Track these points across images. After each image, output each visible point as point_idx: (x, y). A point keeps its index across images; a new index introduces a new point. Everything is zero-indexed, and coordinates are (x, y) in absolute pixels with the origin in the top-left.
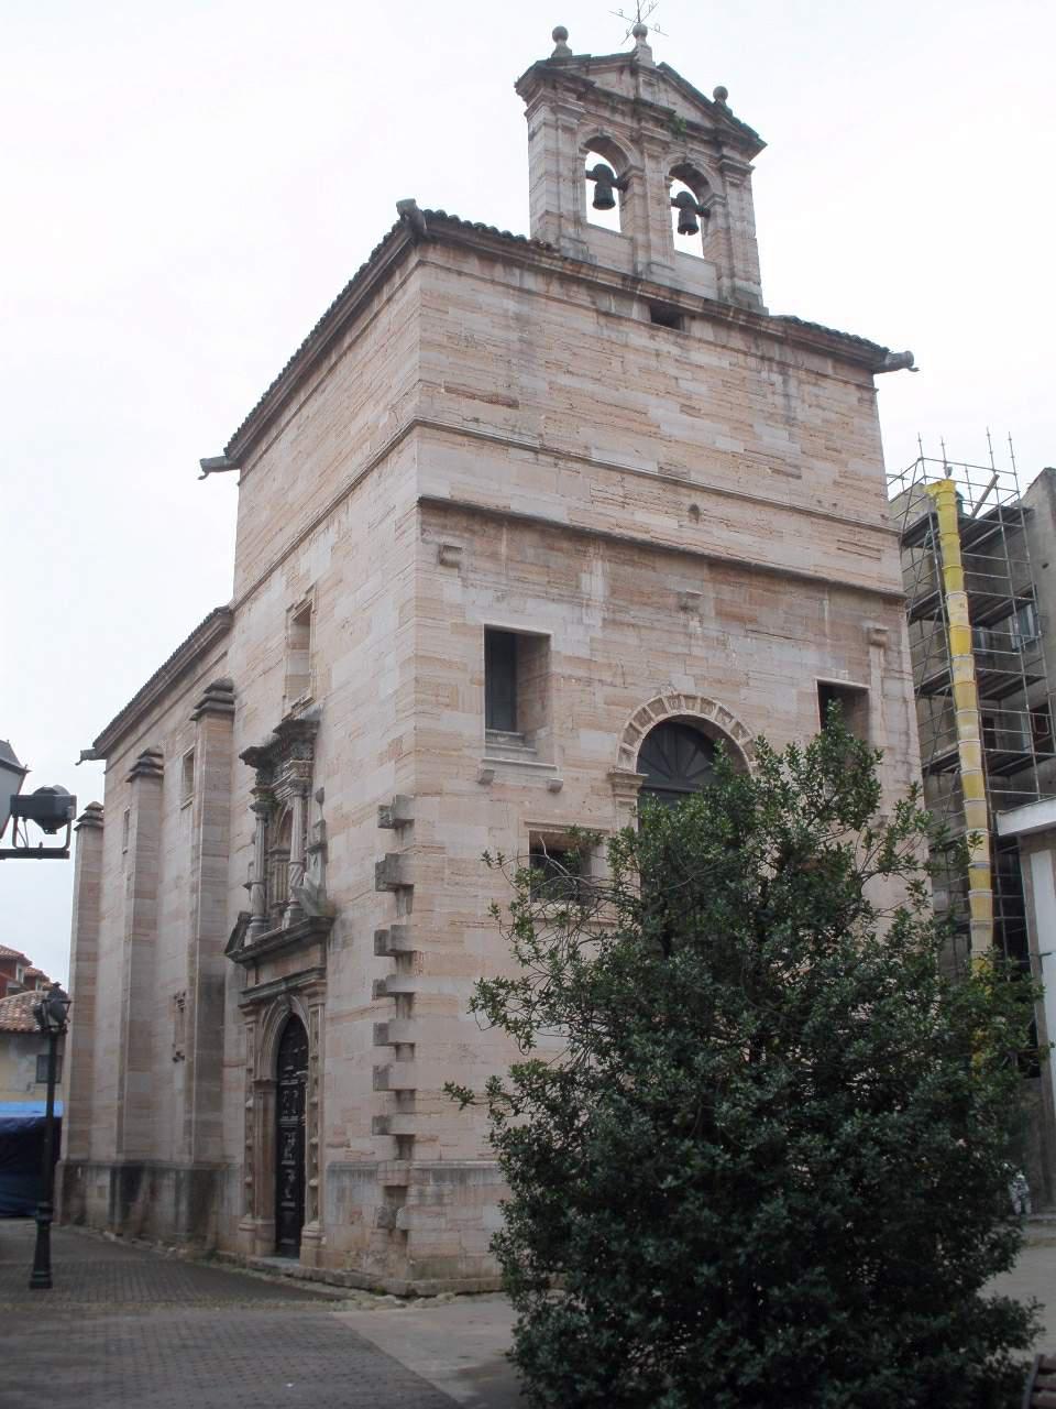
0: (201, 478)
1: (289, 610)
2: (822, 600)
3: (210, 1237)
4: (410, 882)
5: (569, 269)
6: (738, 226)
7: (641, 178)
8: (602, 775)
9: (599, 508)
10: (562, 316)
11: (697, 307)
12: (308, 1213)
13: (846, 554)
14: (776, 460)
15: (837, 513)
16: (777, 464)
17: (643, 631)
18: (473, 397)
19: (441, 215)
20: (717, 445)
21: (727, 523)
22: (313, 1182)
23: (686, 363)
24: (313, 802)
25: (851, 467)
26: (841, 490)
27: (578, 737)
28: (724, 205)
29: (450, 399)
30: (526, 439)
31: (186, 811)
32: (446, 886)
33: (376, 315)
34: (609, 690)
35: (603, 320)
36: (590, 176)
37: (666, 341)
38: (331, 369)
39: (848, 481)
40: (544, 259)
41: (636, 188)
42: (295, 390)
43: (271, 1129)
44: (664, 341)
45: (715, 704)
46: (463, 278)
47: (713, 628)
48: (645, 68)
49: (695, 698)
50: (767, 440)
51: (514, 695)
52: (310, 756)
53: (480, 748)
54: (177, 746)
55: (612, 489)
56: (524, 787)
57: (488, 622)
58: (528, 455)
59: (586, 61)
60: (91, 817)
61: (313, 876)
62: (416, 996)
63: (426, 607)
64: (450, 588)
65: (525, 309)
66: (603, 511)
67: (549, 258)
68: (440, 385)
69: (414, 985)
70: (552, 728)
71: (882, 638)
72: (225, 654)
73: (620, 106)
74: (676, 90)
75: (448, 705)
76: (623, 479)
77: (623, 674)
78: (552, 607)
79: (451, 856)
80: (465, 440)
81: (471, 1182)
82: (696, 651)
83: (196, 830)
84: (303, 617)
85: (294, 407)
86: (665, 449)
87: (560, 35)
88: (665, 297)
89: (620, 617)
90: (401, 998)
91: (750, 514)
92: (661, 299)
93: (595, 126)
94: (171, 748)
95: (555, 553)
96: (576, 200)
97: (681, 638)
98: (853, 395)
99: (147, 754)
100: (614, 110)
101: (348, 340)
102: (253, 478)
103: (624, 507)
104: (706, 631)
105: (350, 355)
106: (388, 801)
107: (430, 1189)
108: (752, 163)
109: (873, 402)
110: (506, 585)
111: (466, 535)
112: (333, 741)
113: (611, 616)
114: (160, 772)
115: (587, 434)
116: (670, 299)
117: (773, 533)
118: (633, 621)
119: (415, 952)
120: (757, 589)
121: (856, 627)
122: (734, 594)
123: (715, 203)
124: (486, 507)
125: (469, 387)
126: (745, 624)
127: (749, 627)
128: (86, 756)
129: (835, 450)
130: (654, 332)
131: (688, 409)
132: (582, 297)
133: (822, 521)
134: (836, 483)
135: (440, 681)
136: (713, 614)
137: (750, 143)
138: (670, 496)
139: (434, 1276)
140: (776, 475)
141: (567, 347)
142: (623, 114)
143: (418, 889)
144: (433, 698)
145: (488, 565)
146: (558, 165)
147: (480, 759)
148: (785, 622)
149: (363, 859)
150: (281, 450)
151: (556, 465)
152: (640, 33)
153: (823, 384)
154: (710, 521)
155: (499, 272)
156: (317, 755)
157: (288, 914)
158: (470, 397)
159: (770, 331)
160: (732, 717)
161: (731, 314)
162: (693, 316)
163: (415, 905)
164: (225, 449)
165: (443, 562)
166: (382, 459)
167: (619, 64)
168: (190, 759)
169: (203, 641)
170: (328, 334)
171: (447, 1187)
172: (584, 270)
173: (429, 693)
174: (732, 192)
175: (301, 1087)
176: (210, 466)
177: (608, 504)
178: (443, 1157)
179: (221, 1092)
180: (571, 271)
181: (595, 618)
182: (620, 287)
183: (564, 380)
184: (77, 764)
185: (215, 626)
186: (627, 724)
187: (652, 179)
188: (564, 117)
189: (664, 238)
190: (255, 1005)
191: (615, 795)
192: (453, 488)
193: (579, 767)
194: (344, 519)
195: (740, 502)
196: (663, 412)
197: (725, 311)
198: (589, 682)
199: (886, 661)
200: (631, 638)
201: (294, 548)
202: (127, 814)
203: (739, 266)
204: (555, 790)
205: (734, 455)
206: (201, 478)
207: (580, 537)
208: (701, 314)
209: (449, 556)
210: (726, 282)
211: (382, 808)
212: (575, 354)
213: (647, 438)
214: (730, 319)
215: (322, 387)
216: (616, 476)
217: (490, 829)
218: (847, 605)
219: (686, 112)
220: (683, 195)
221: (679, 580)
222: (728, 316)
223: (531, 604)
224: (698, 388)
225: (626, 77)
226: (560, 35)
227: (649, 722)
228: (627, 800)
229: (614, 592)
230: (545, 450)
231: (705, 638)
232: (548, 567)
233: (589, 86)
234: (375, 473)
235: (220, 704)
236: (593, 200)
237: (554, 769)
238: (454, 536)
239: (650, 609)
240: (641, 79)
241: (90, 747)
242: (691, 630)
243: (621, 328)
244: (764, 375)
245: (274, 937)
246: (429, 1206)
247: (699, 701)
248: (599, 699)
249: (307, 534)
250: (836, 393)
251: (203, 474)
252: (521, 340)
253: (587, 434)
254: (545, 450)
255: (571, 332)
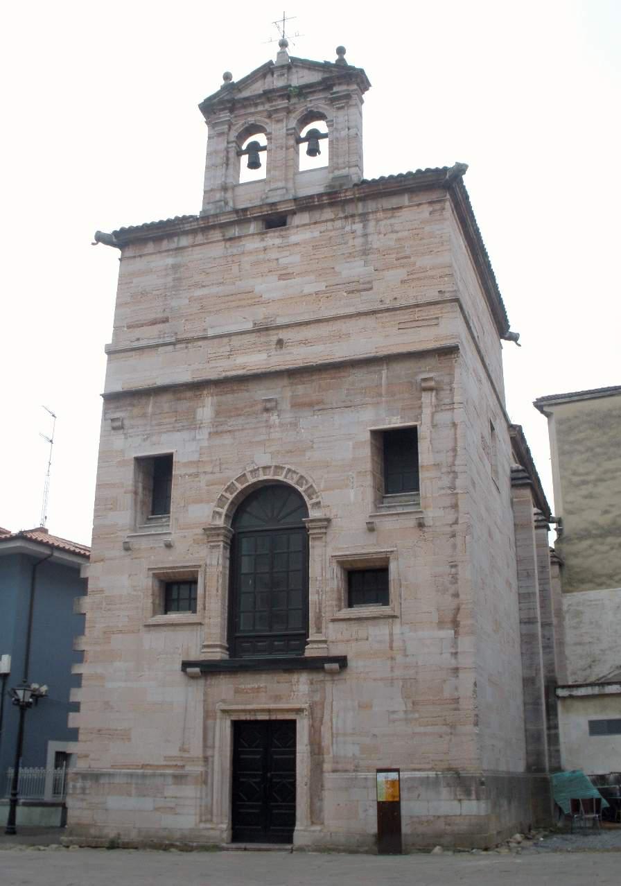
2: (380, 371)
4: (85, 612)
5: (202, 224)
8: (200, 531)
9: (213, 364)
11: (291, 207)
14: (339, 286)
15: (397, 304)
16: (353, 287)
18: (142, 326)
19: (123, 230)
21: (305, 342)
27: (187, 510)
29: (130, 332)
32: (104, 612)
34: (209, 477)
39: (415, 276)
40: (186, 225)
45: (285, 468)
46: (143, 258)
47: (288, 417)
49: (270, 467)
56: (151, 548)
57: (136, 455)
58: (170, 348)
64: (119, 441)
65: (179, 259)
67: (188, 223)
68: (124, 327)
71: (432, 384)
73: (258, 101)
74: (303, 67)
77: (220, 464)
78: (178, 435)
79: (107, 594)
80: (133, 353)
81: (102, 781)
91: (324, 330)
92: (266, 213)
93: (243, 122)
97: (264, 430)
100: (256, 105)
107: (79, 785)
111: (129, 408)
116: (272, 210)
117: (340, 337)
118: (230, 429)
119: (84, 651)
120: (325, 380)
121: (411, 382)
122: (304, 389)
125: (140, 320)
126: (313, 407)
127: (317, 408)
129: (406, 257)
131: (284, 276)
133: (387, 314)
136: (288, 407)
138: (263, 339)
139: (77, 835)
142: (263, 103)
148: (347, 396)
151: (187, 347)
154: (291, 346)
155: (165, 245)
158: (140, 327)
159: (348, 197)
162: (293, 213)
167: (261, 74)
171: (88, 784)
172: (210, 220)
177: (219, 359)
178: (92, 766)
180: (204, 223)
181: (203, 435)
182: (237, 219)
191: (209, 542)
193: (187, 529)
195: (317, 325)
197: (310, 200)
198: (197, 475)
199: (437, 399)
200: (227, 439)
208: (296, 209)
212: (208, 273)
216: (226, 340)
217: (130, 576)
218: (401, 369)
221: (261, 392)
222: (314, 202)
223: (164, 437)
226: (341, 51)
227: (235, 491)
228: (216, 544)
230: (179, 341)
231: (281, 425)
232: (176, 412)
237: (170, 533)
238: (122, 411)
239: (243, 417)
242: (271, 422)
243: (241, 243)
244: (348, 228)
248: (203, 484)
252: (174, 280)
254: (179, 341)
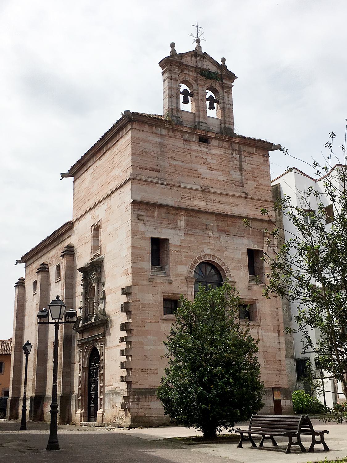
0: (61, 179)
1: (92, 226)
3: (67, 417)
6: (227, 106)
7: (197, 93)
8: (183, 278)
10: (172, 142)
12: (99, 407)
13: (257, 210)
15: (255, 197)
17: (196, 236)
20: (218, 179)
21: (221, 203)
22: (101, 397)
23: (210, 154)
24: (101, 284)
25: (260, 182)
26: (256, 190)
28: (223, 99)
30: (162, 182)
31: (57, 284)
33: (118, 141)
34: (185, 254)
35: (185, 143)
36: (181, 93)
37: (204, 147)
38: (104, 153)
41: (195, 97)
42: (92, 157)
43: (87, 383)
44: (203, 148)
47: (216, 234)
48: (199, 55)
49: (211, 255)
50: (234, 176)
51: (159, 255)
52: (100, 271)
53: (150, 272)
54: (54, 262)
55: (187, 195)
59: (182, 55)
60: (21, 283)
61: (101, 306)
62: (132, 342)
63: (135, 233)
64: (141, 227)
65: (162, 141)
66: (184, 201)
69: (132, 339)
70: (169, 266)
72: (71, 236)
75: (141, 260)
76: (190, 191)
79: (142, 302)
82: (211, 241)
83: (63, 291)
84: (97, 229)
85: (92, 162)
86: (203, 181)
87: (173, 45)
88: (203, 134)
89: (189, 232)
90: (128, 343)
91: (228, 200)
94: (51, 262)
95: (170, 215)
96: (177, 103)
97: (207, 238)
98: (262, 159)
99: (43, 264)
101: (109, 146)
102: (78, 181)
103: (190, 200)
104: (214, 235)
105: (110, 151)
106: (124, 287)
108: (232, 84)
109: (268, 161)
110: (157, 225)
112: (107, 267)
113: (187, 232)
114: (47, 270)
115: (180, 178)
118: (193, 234)
122: (223, 224)
123: (220, 99)
124: (162, 448)
127: (227, 233)
128: (18, 262)
129: (255, 177)
130: (200, 145)
131: (210, 169)
132: (179, 135)
134: (255, 188)
135: (138, 253)
137: (232, 77)
140: (236, 187)
141: (174, 152)
143: (133, 312)
144: (137, 258)
145: (152, 220)
146: (172, 92)
147: (149, 275)
149: (117, 302)
150: (88, 176)
151: (171, 189)
152: (198, 41)
153: (252, 157)
156: (102, 271)
157: (94, 318)
160: (221, 260)
161: (224, 137)
163: (132, 317)
164: (69, 171)
165: (139, 219)
166: (121, 187)
168: (58, 268)
169: (63, 231)
170: (103, 142)
173: (136, 257)
174: (226, 95)
175: (97, 369)
176: (63, 175)
177: (186, 199)
179: (71, 371)
181: (181, 233)
183: (173, 162)
184: (15, 265)
185: (67, 227)
186: (191, 264)
187: (201, 93)
188: (174, 75)
189: (204, 113)
190: (82, 345)
192: (141, 197)
194: (109, 202)
196: (203, 170)
200: (192, 239)
201: (93, 207)
202: (35, 283)
203: (227, 119)
204: (170, 283)
205: (224, 181)
206: (61, 179)
207: (178, 209)
209: (141, 218)
210: (223, 125)
211: (122, 289)
213: (197, 178)
214: (223, 139)
215: (101, 158)
217: (153, 295)
219: (213, 69)
220: (211, 97)
223: (164, 230)
224: (213, 162)
225: (193, 58)
226: (173, 45)
229: (187, 225)
232: (169, 219)
233: (182, 64)
234: (119, 191)
235: (70, 252)
236: (182, 101)
240: (198, 59)
241: (20, 259)
242: (210, 235)
244: (234, 155)
245: (89, 324)
246: (136, 402)
247: (212, 256)
249: (98, 204)
250: (257, 159)
251: (62, 178)
252: (161, 151)
253: (180, 178)
254: (167, 184)
255: (175, 147)
